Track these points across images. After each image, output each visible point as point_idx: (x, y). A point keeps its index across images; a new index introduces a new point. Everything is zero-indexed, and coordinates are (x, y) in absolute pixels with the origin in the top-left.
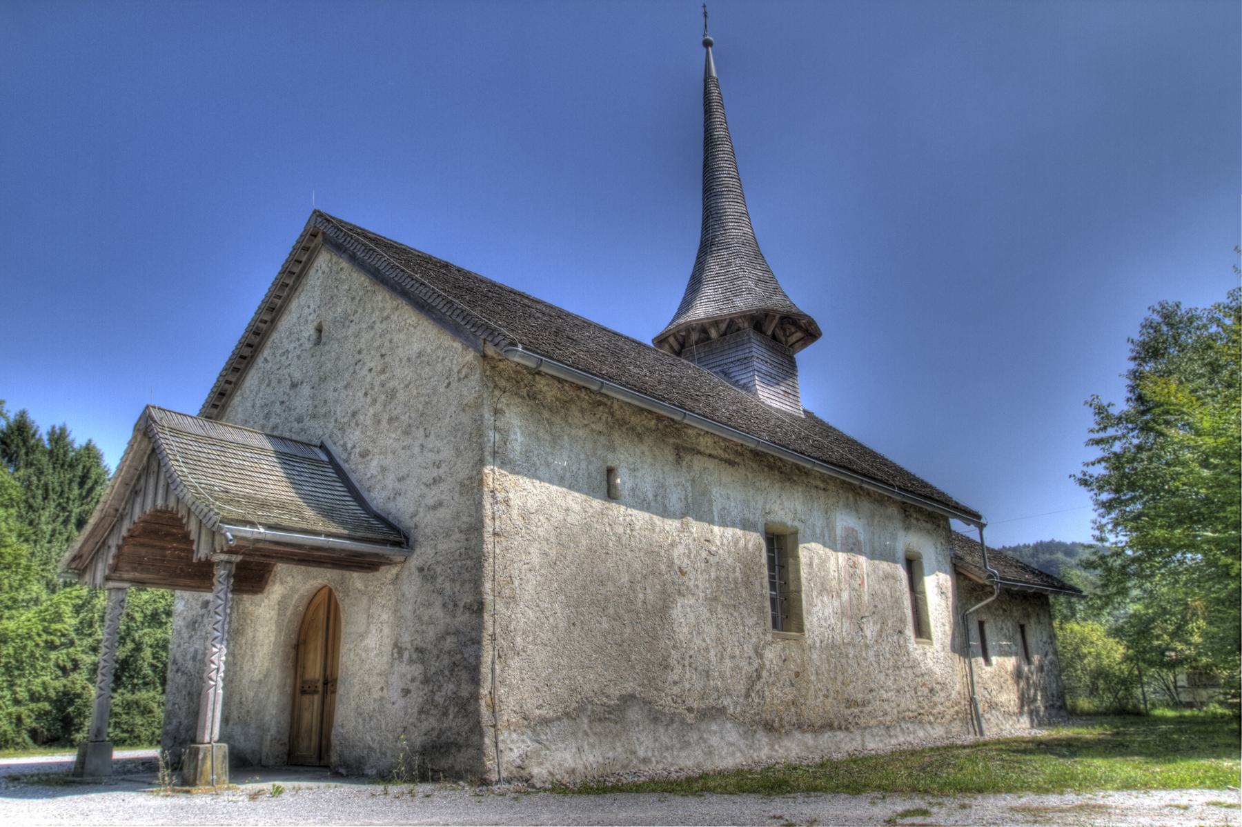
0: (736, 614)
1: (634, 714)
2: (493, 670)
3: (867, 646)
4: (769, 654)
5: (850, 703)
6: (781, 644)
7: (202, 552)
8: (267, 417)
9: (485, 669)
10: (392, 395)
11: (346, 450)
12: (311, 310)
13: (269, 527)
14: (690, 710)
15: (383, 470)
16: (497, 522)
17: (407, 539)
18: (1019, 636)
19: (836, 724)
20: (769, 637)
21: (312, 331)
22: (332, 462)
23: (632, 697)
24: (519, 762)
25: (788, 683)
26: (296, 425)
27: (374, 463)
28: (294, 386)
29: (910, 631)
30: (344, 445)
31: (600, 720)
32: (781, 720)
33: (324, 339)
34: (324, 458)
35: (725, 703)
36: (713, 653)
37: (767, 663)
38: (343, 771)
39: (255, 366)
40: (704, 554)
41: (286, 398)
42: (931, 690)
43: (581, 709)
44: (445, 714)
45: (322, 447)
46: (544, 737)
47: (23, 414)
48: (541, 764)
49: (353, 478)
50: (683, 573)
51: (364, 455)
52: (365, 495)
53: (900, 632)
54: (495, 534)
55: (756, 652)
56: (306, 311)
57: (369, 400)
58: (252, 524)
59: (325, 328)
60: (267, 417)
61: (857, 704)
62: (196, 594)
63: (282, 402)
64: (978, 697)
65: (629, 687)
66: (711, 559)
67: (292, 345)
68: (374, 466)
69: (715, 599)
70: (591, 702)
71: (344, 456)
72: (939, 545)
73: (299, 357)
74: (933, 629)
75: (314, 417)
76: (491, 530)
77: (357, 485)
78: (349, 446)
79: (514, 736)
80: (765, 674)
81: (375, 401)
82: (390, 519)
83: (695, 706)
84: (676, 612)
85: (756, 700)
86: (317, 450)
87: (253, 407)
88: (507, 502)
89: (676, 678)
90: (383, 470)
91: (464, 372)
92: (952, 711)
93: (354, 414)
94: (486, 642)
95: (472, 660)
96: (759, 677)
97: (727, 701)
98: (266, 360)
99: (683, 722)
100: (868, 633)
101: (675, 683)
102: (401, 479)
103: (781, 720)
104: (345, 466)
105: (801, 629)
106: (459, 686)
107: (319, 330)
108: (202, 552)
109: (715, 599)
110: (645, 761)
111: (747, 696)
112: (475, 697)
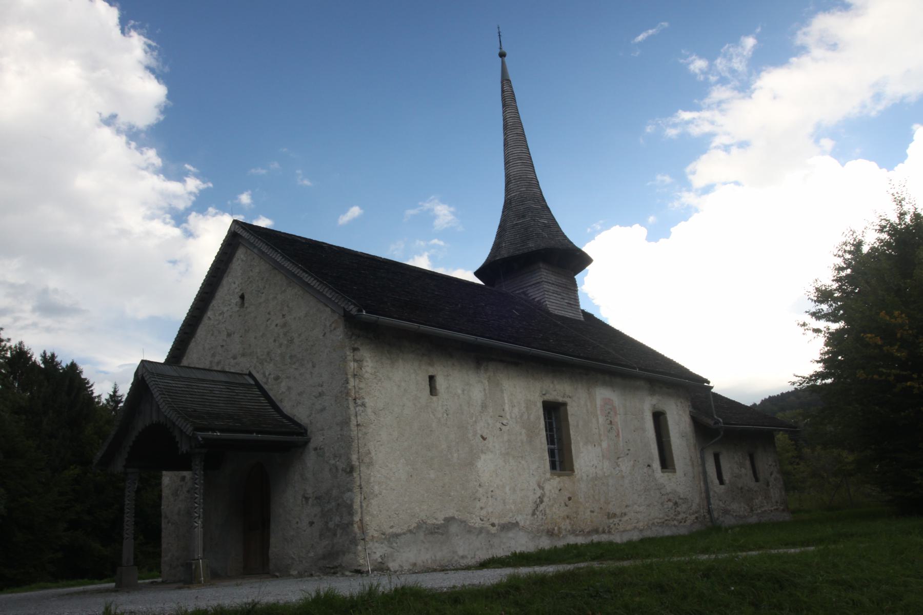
0: (523, 462)
1: (454, 528)
2: (361, 507)
3: (623, 477)
4: (547, 487)
5: (611, 516)
6: (558, 479)
7: (184, 448)
8: (213, 355)
9: (356, 506)
10: (291, 341)
11: (265, 376)
12: (236, 286)
13: (221, 431)
14: (493, 525)
15: (289, 388)
16: (359, 418)
17: (306, 430)
18: (748, 463)
19: (601, 529)
20: (548, 475)
21: (238, 300)
22: (257, 384)
23: (453, 518)
24: (380, 560)
25: (563, 504)
26: (232, 360)
27: (283, 384)
28: (229, 335)
29: (656, 465)
30: (264, 374)
31: (432, 533)
32: (559, 528)
33: (246, 305)
34: (252, 382)
35: (518, 519)
36: (507, 488)
37: (547, 493)
38: (277, 574)
39: (203, 323)
40: (499, 425)
41: (224, 344)
42: (676, 504)
43: (419, 527)
44: (335, 535)
45: (250, 375)
46: (395, 545)
47: (21, 343)
48: (394, 560)
49: (271, 394)
50: (484, 439)
51: (277, 378)
52: (279, 404)
53: (649, 466)
54: (358, 425)
55: (539, 486)
56: (233, 286)
57: (277, 344)
58: (213, 430)
59: (246, 297)
60: (213, 355)
61: (615, 515)
62: (176, 473)
63: (222, 346)
64: (713, 506)
65: (451, 513)
66: (503, 428)
67: (226, 309)
68: (283, 386)
69: (508, 454)
70: (425, 523)
71: (264, 380)
72: (679, 404)
73: (231, 316)
74: (676, 462)
75: (243, 355)
76: (355, 423)
77: (273, 398)
78: (267, 374)
79: (376, 545)
80: (546, 499)
81: (281, 345)
82: (296, 419)
83: (496, 522)
84: (480, 464)
85: (540, 517)
86: (247, 377)
87: (204, 349)
88: (363, 405)
89: (482, 505)
90: (289, 388)
91: (333, 325)
92: (693, 517)
93: (268, 353)
94: (356, 490)
95: (348, 502)
96: (542, 502)
97: (519, 518)
98: (209, 318)
99: (488, 532)
100: (623, 468)
101: (482, 508)
102: (300, 394)
103: (559, 528)
104: (265, 387)
105: (572, 470)
106: (341, 517)
107: (242, 297)
108: (184, 448)
109: (508, 454)
110: (463, 557)
111: (534, 514)
112: (351, 523)
